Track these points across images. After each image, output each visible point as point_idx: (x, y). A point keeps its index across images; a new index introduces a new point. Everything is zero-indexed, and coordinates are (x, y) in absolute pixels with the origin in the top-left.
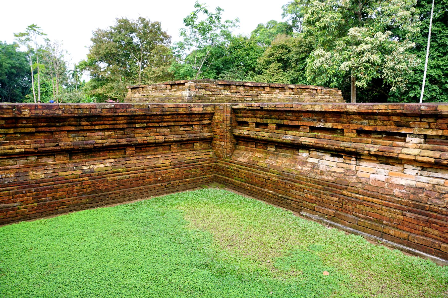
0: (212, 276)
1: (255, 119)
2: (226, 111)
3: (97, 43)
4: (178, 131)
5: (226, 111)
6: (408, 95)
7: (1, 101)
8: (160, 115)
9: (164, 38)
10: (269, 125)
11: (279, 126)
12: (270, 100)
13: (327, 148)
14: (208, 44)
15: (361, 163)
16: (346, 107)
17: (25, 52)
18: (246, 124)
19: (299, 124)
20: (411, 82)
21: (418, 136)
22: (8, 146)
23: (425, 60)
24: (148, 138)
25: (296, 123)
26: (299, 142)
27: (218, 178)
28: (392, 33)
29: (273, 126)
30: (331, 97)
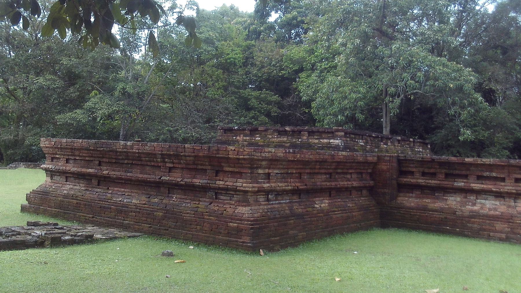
0: (12, 212)
1: (421, 170)
2: (392, 161)
3: (511, 19)
4: (459, 86)
5: (392, 161)
6: (289, 16)
7: (520, 223)
8: (350, 163)
9: (177, 94)
10: (414, 173)
11: (447, 176)
12: (228, 136)
13: (428, 198)
14: (450, 21)
15: (518, 201)
16: (509, 162)
17: (227, 5)
18: (412, 173)
19: (468, 173)
20: (260, 124)
21: (325, 174)
22: (478, 185)
23: (455, 156)
24: (227, 183)
25: (464, 172)
26: (470, 188)
27: (240, 161)
28: (461, 138)
29: (442, 176)
30: (379, 272)
